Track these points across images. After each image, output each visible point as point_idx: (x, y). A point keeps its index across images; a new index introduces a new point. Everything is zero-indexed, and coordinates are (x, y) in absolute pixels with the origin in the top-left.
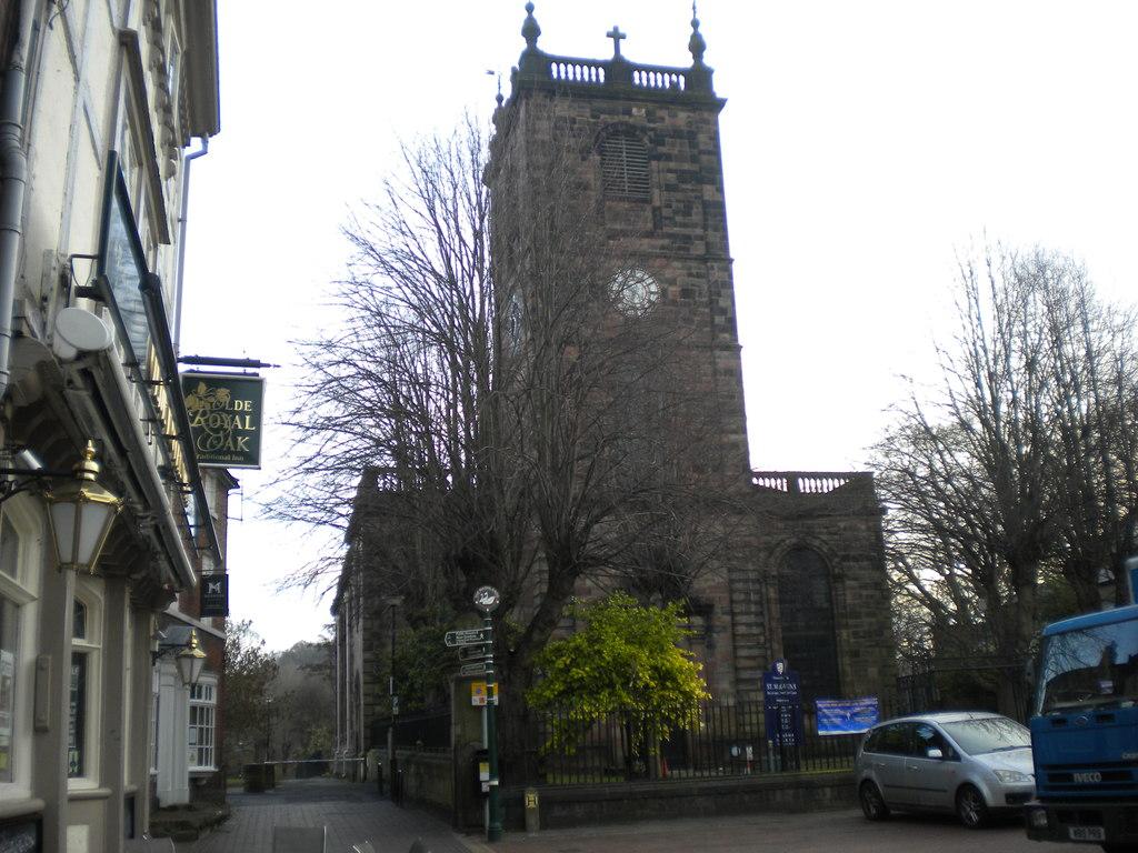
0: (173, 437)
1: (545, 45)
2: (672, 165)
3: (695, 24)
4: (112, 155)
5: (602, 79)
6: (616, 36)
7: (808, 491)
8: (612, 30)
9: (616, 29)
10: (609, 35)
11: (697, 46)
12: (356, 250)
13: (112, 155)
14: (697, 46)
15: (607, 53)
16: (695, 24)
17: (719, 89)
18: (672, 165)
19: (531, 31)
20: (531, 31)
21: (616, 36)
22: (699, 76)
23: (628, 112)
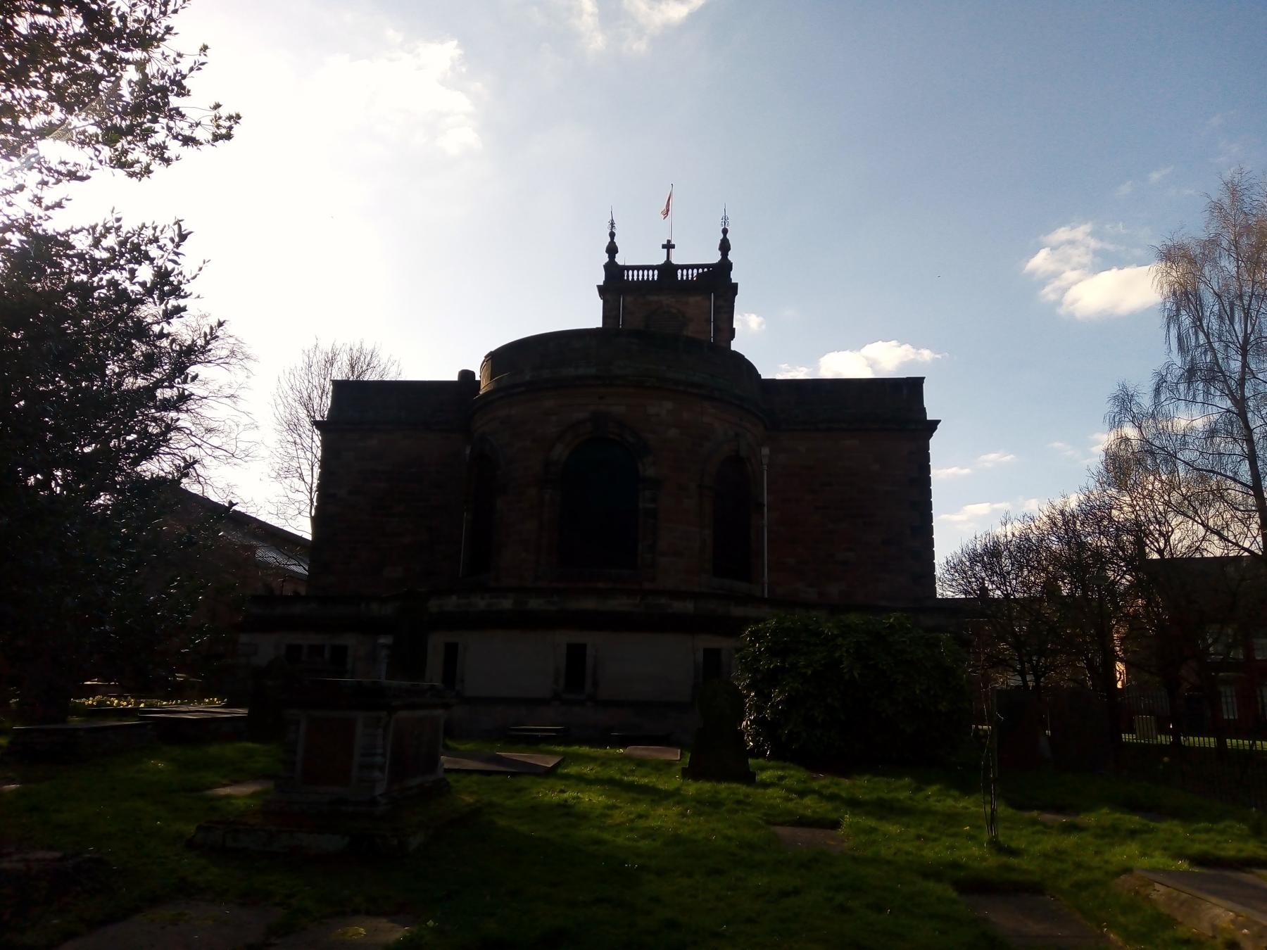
0: (141, 128)
1: (620, 260)
3: (725, 231)
4: (1200, 860)
5: (656, 278)
6: (669, 246)
7: (1202, 745)
8: (666, 243)
9: (664, 247)
10: (664, 247)
11: (725, 247)
12: (188, 294)
13: (1200, 860)
14: (725, 247)
15: (660, 259)
16: (725, 231)
17: (735, 277)
19: (612, 250)
20: (612, 250)
21: (669, 246)
22: (724, 267)
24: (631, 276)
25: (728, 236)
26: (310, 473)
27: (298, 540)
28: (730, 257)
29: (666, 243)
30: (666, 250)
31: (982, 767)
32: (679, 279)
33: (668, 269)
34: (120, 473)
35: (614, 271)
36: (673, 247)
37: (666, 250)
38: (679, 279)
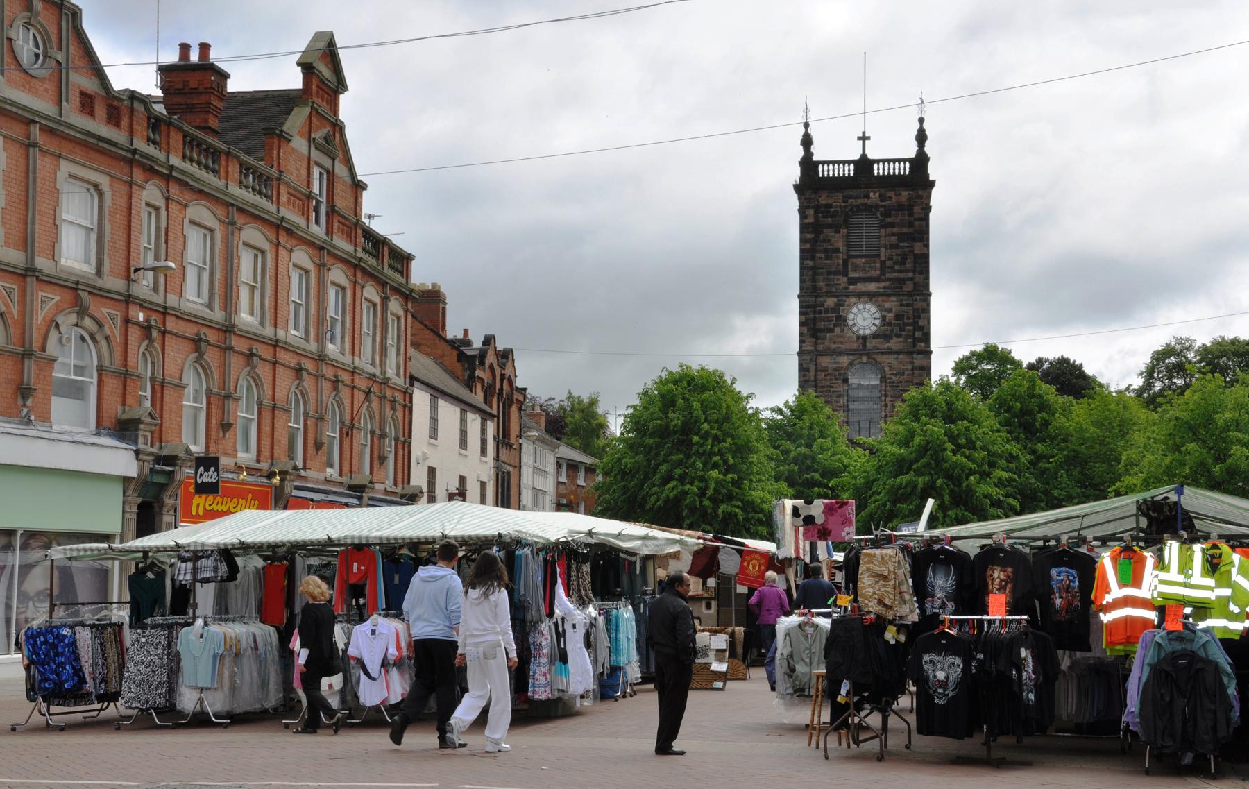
2: (895, 230)
3: (921, 120)
6: (864, 138)
8: (861, 135)
9: (859, 138)
10: (859, 138)
11: (921, 137)
14: (921, 137)
16: (921, 120)
18: (895, 230)
19: (807, 142)
20: (807, 142)
21: (864, 138)
22: (920, 162)
23: (867, 196)
24: (878, 170)
25: (925, 125)
26: (165, 372)
27: (54, 395)
28: (928, 149)
29: (861, 135)
30: (861, 142)
31: (296, 631)
32: (821, 175)
33: (864, 164)
34: (30, 644)
35: (808, 165)
36: (869, 138)
37: (861, 142)
38: (821, 175)
